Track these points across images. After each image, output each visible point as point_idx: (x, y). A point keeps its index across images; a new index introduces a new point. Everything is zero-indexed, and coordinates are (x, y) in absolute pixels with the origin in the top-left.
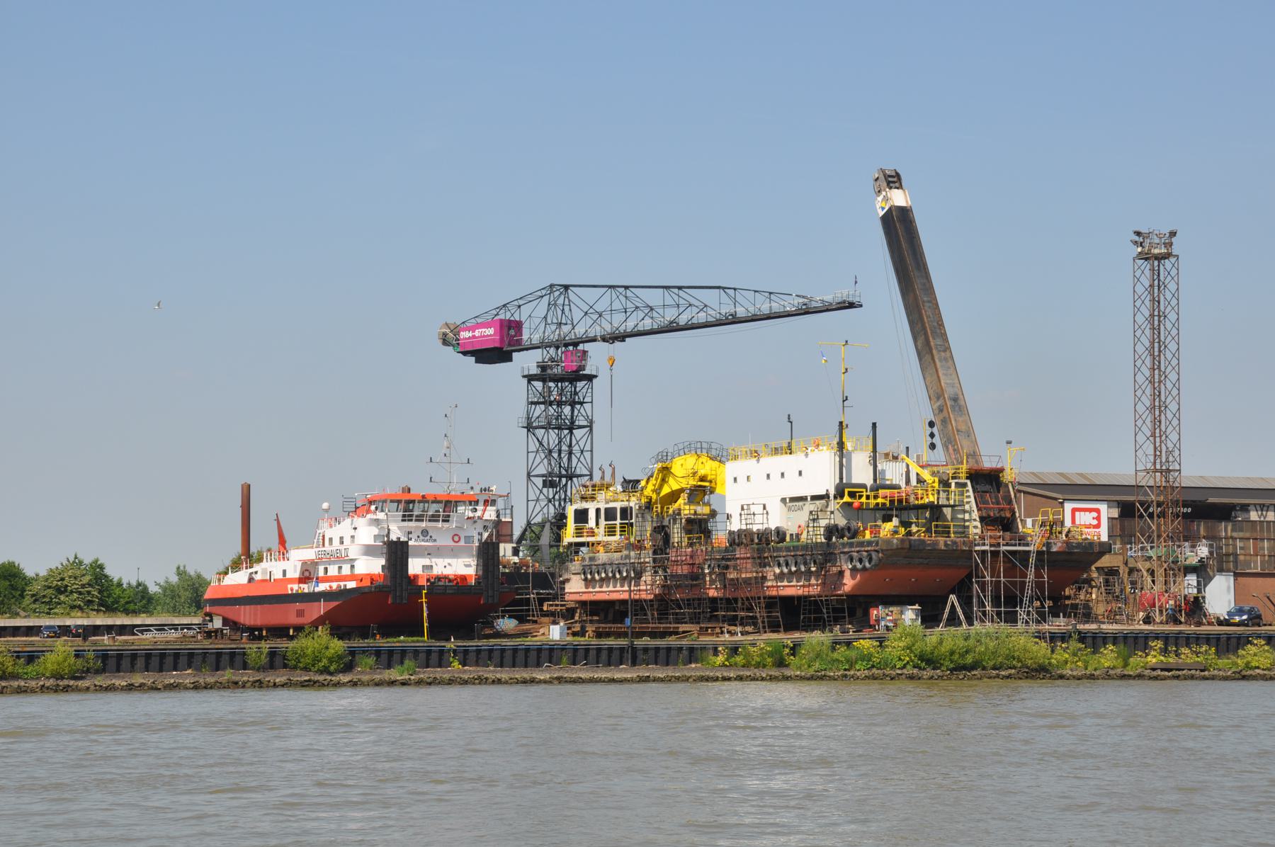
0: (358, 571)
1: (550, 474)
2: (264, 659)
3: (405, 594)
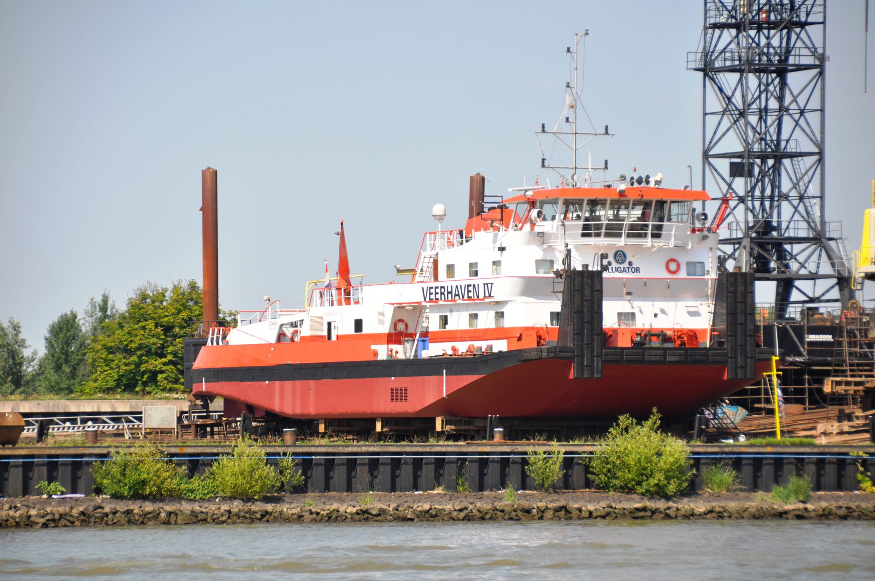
0: (508, 322)
1: (748, 153)
2: (556, 471)
3: (597, 363)
